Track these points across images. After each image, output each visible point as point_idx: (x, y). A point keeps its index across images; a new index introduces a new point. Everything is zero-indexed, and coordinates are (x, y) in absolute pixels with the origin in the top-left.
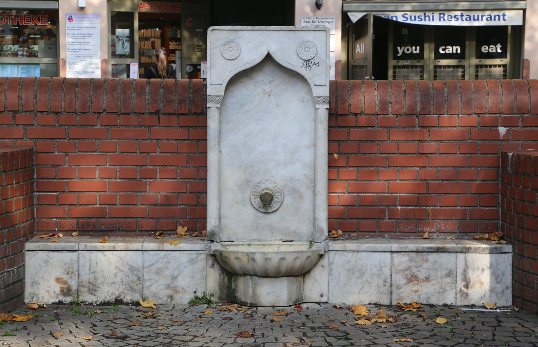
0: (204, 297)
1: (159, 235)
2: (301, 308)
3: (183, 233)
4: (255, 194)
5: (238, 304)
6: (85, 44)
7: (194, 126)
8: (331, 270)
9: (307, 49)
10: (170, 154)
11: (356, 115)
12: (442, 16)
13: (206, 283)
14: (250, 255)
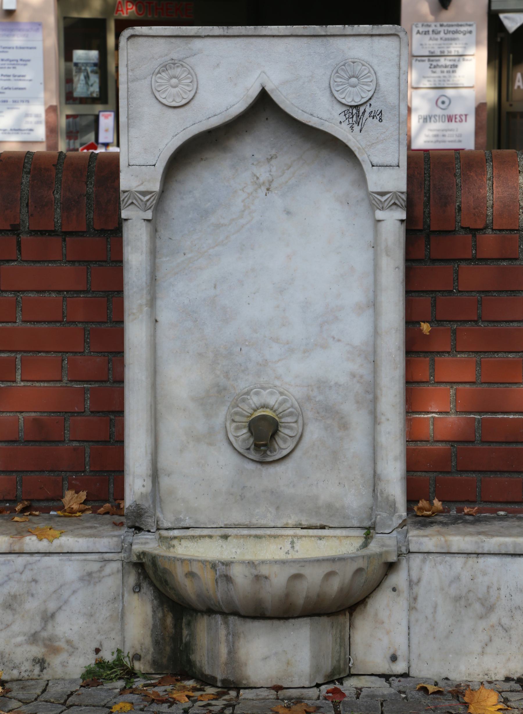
0: (119, 662)
1: (23, 511)
2: (343, 695)
3: (75, 507)
4: (237, 418)
5: (197, 680)
6: (16, 78)
7: (99, 261)
8: (415, 599)
9: (354, 80)
10: (45, 326)
11: (473, 231)
13: (122, 630)
14: (220, 567)
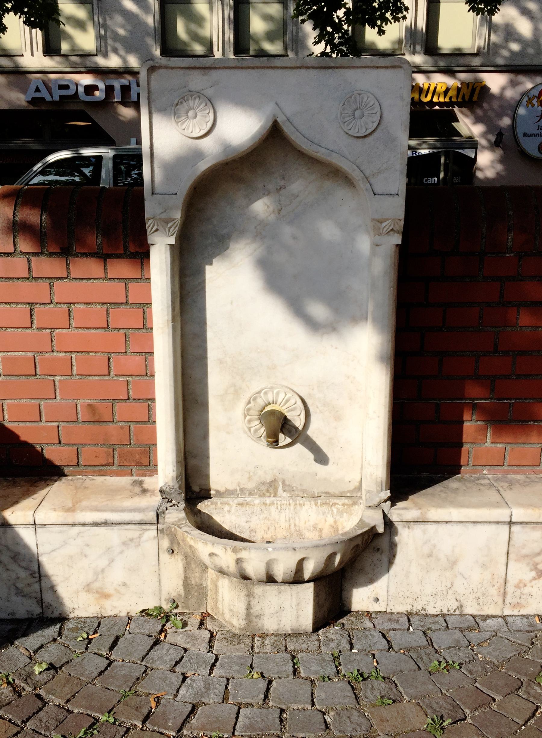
12: (414, 153)
